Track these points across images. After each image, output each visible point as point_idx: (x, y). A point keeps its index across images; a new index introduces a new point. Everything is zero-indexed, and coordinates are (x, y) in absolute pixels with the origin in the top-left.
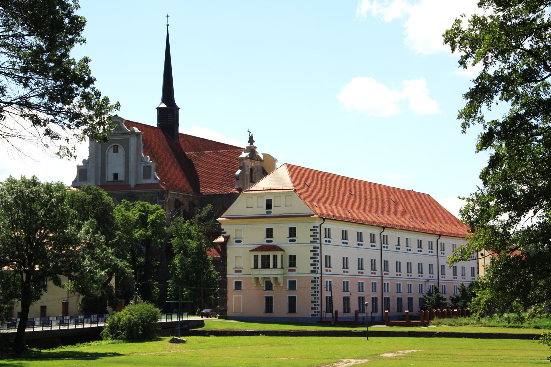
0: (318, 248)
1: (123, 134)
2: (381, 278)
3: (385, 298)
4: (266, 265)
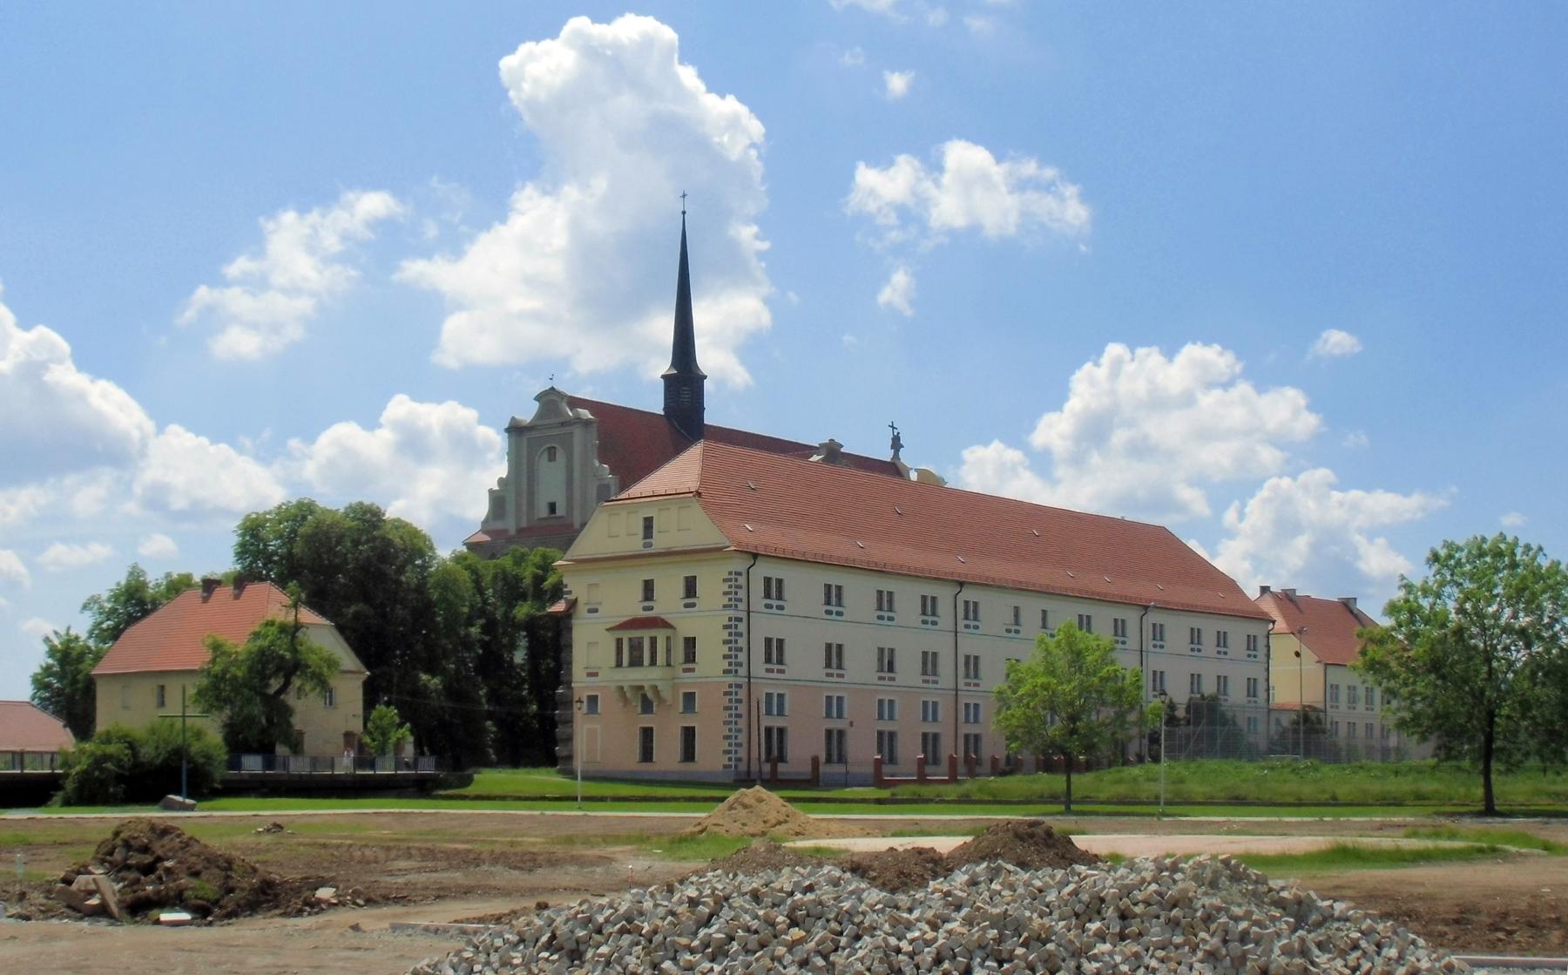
0: (740, 620)
1: (563, 424)
2: (954, 692)
3: (967, 737)
4: (636, 662)
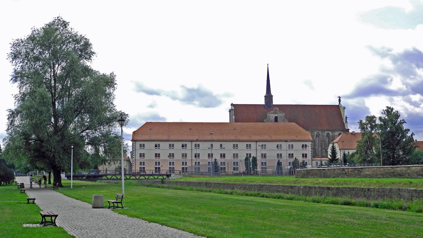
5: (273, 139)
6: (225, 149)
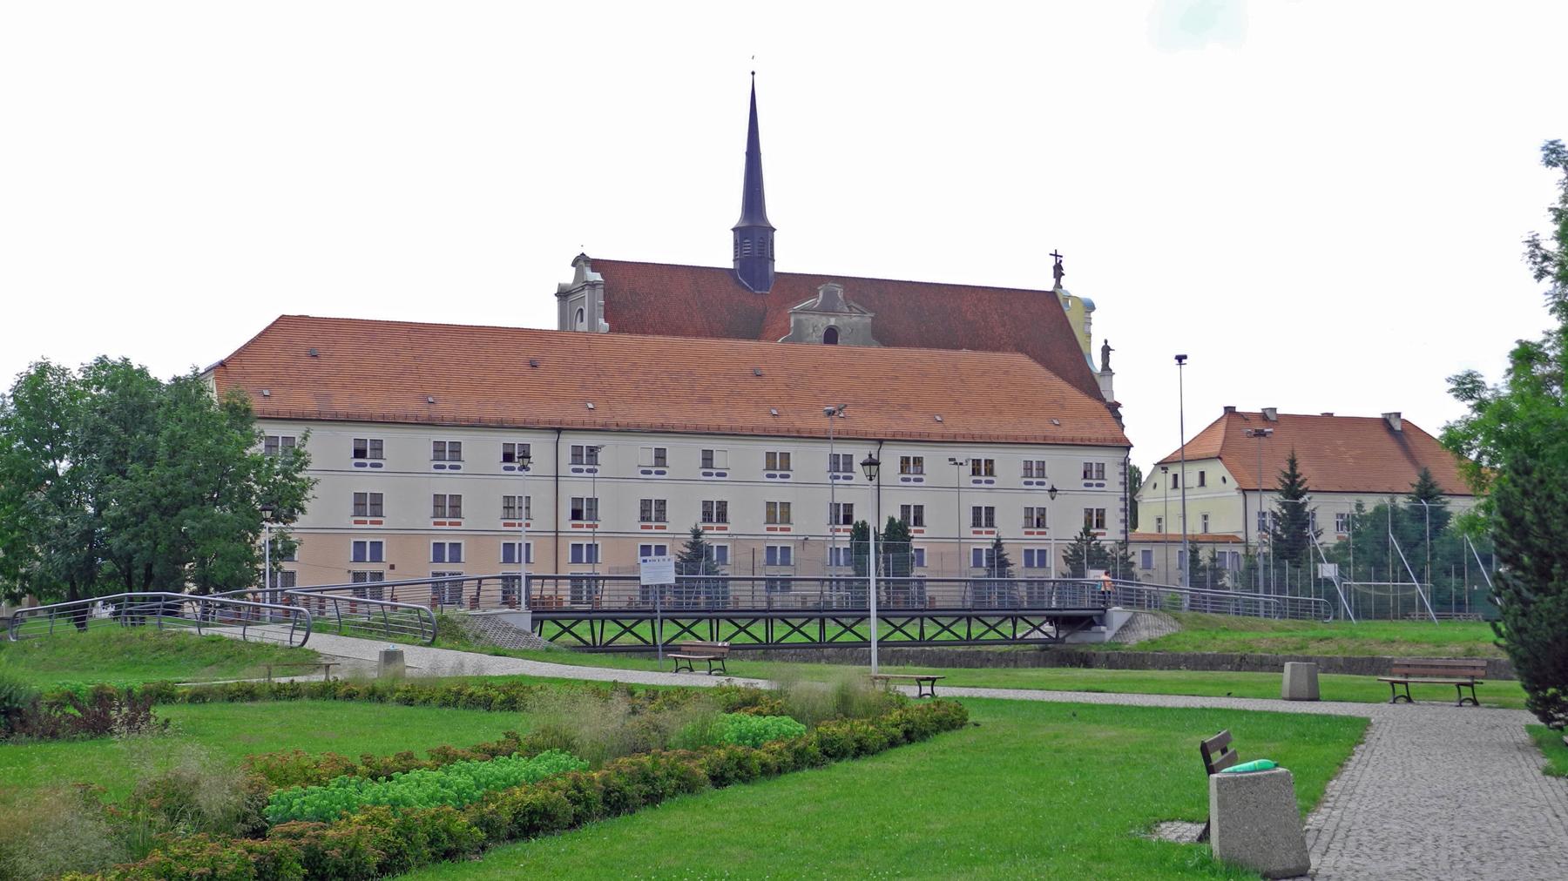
2: (554, 534)
5: (953, 431)
6: (725, 475)
